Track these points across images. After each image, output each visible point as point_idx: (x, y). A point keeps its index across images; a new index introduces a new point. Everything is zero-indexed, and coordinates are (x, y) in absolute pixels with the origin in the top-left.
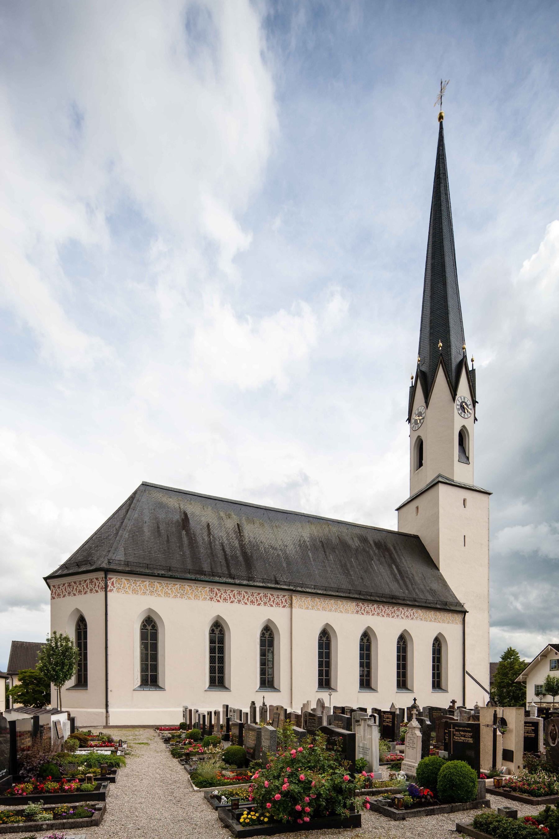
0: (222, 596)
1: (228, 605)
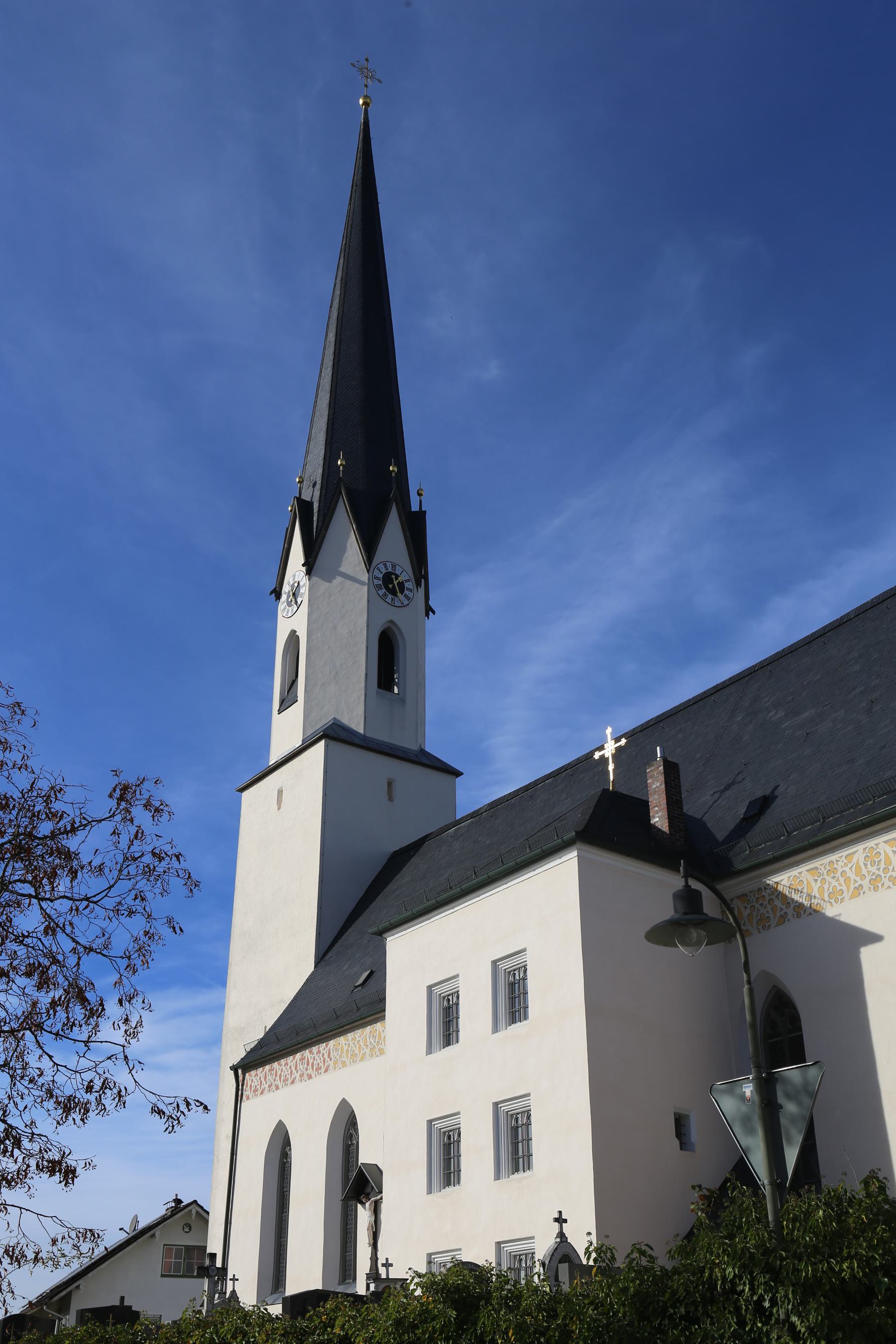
0: (826, 886)
1: (285, 1092)
